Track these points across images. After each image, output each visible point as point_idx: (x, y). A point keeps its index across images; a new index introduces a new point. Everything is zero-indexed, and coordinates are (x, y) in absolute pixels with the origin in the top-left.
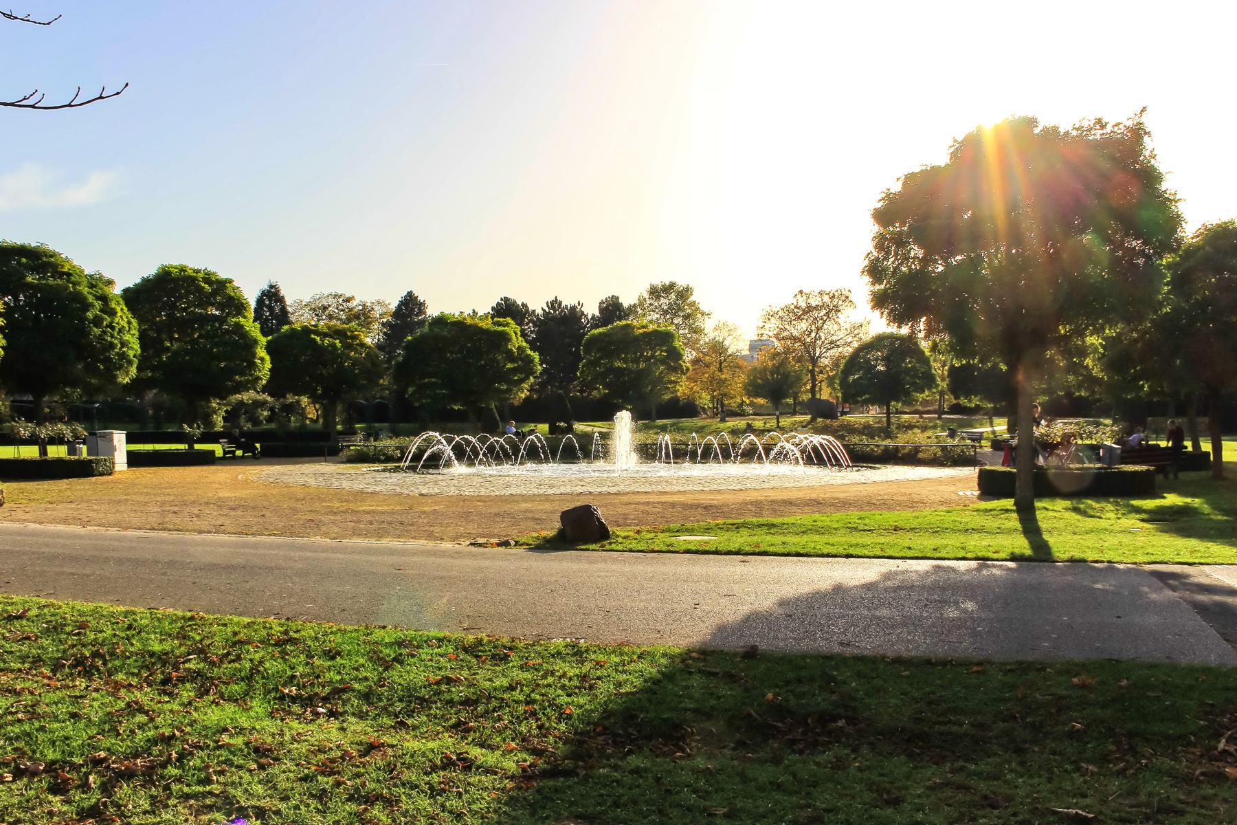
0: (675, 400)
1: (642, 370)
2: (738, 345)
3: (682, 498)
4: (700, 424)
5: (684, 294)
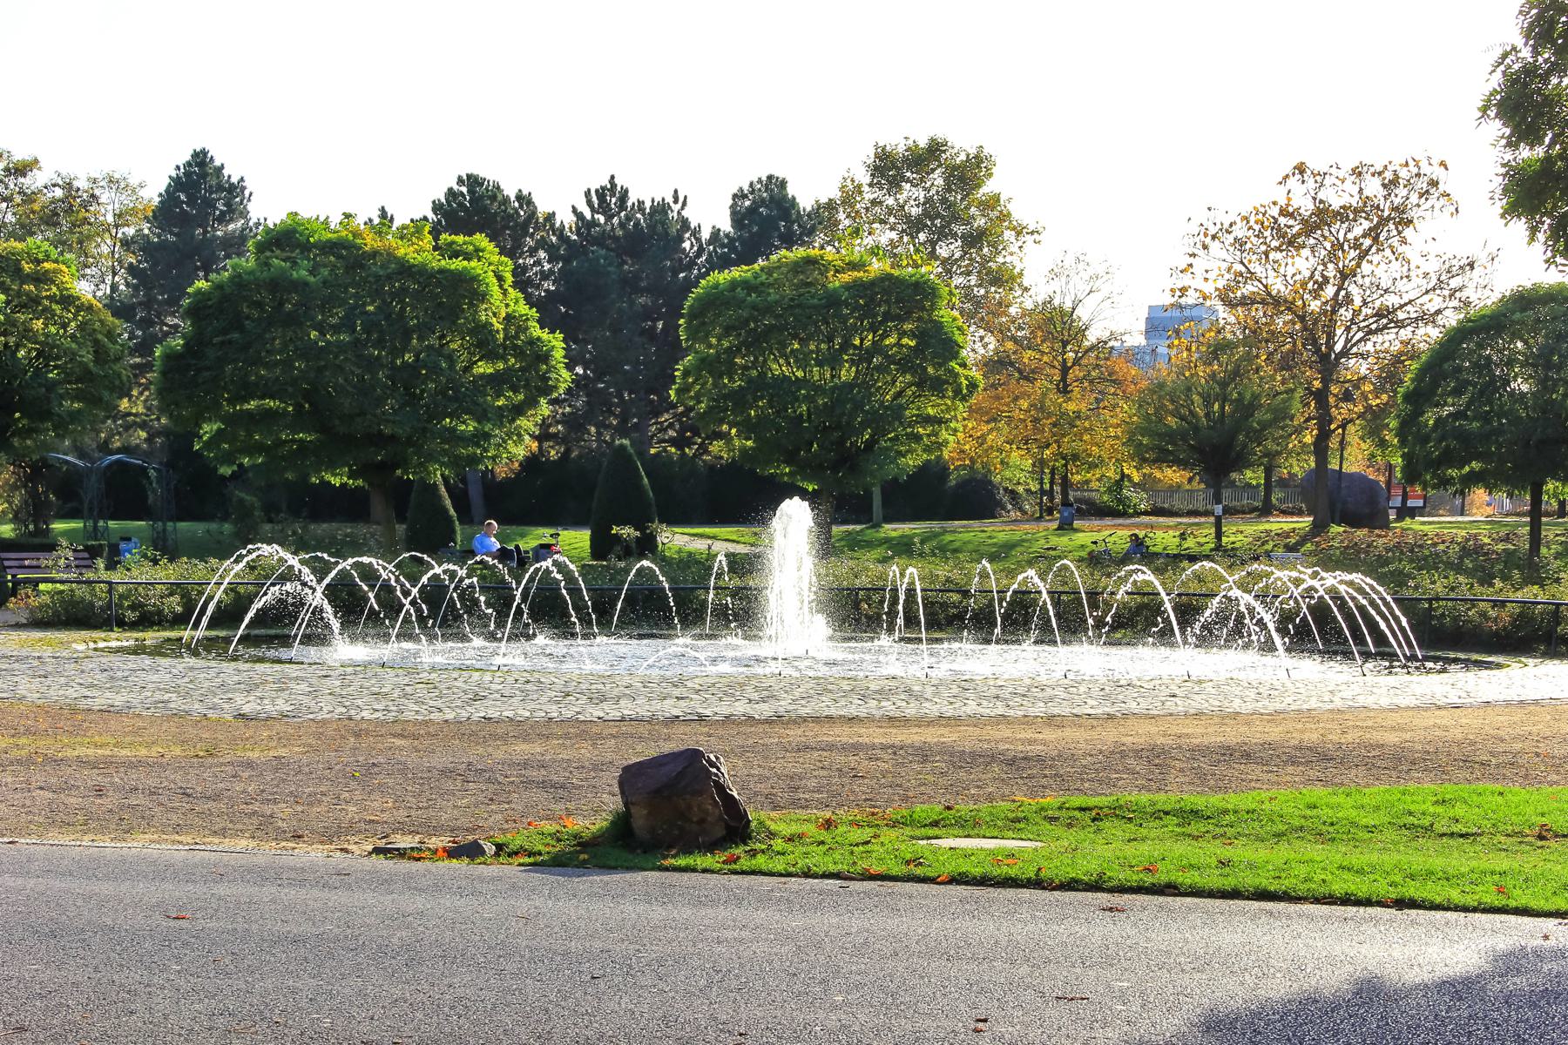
0: (933, 474)
1: (849, 386)
2: (1117, 317)
3: (948, 736)
4: (1002, 537)
5: (968, 173)
